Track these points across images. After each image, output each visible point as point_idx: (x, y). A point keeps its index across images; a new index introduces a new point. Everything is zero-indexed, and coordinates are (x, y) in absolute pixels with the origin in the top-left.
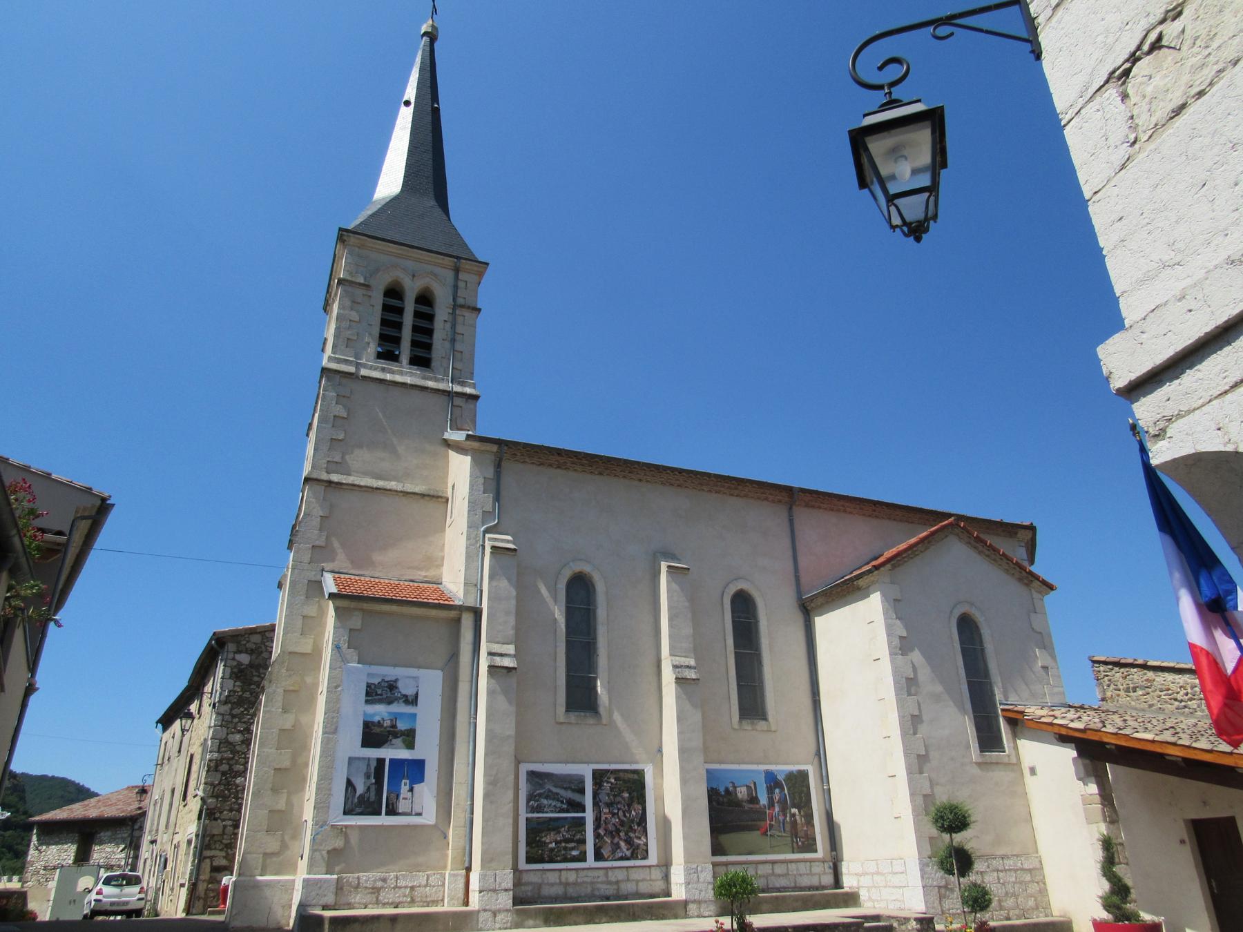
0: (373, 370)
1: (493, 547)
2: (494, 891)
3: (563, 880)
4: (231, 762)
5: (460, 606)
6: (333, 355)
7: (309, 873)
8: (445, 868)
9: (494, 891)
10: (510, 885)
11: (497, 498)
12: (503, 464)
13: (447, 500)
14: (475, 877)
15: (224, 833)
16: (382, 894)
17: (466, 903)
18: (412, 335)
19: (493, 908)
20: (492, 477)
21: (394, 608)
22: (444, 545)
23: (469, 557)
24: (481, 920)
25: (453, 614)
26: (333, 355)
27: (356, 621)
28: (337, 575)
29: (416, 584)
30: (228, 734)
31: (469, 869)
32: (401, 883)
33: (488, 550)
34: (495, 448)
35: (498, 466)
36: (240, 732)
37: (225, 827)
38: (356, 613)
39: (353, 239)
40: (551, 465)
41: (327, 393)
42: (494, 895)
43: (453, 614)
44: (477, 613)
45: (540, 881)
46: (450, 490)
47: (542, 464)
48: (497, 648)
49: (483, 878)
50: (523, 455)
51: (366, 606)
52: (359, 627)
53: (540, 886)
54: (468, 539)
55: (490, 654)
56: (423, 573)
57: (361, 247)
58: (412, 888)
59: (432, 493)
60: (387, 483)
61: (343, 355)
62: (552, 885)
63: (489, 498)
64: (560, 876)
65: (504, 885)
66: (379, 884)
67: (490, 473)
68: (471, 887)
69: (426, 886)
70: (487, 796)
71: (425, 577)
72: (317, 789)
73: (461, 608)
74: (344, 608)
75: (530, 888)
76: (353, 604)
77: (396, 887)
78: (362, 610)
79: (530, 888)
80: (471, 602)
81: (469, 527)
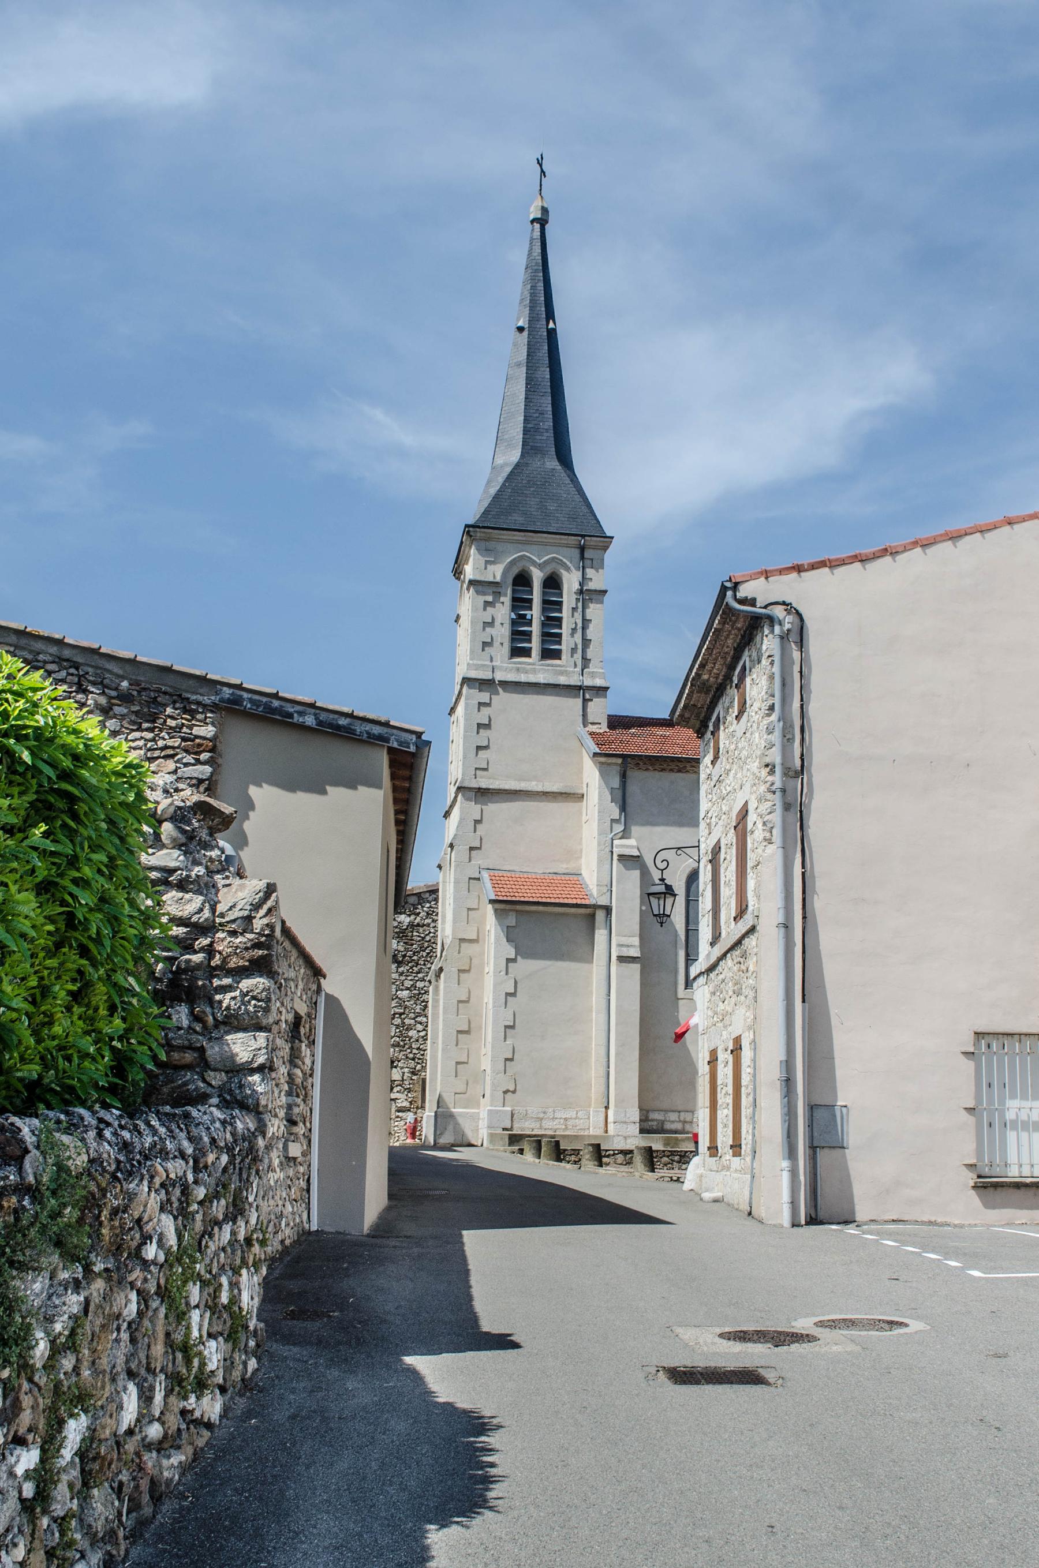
0: (507, 670)
1: (619, 856)
2: (625, 1122)
3: (682, 1119)
4: (403, 1016)
5: (594, 905)
6: (471, 662)
7: (491, 1106)
8: (590, 1106)
9: (625, 1122)
10: (637, 1119)
11: (623, 808)
12: (629, 773)
13: (583, 795)
14: (611, 1112)
15: (403, 1080)
16: (544, 1122)
17: (606, 1132)
18: (543, 592)
19: (624, 1134)
20: (618, 787)
21: (541, 908)
22: (581, 838)
23: (600, 861)
24: (615, 1142)
25: (588, 911)
26: (471, 662)
27: (511, 920)
28: (492, 873)
29: (559, 877)
30: (397, 991)
31: (607, 1108)
32: (558, 1115)
33: (615, 857)
34: (620, 761)
35: (624, 776)
36: (407, 989)
37: (404, 1073)
38: (511, 913)
39: (479, 533)
40: (671, 770)
41: (469, 701)
42: (625, 1126)
43: (588, 911)
44: (608, 910)
45: (663, 1118)
46: (585, 786)
47: (663, 770)
48: (624, 940)
49: (616, 1113)
50: (645, 764)
51: (519, 907)
52: (514, 924)
53: (663, 1122)
54: (599, 844)
55: (620, 945)
56: (565, 866)
57: (488, 539)
58: (566, 1119)
59: (568, 791)
60: (528, 783)
61: (480, 660)
62: (673, 1122)
63: (615, 812)
64: (679, 1116)
65: (632, 1119)
66: (541, 1115)
67: (616, 782)
68: (609, 1120)
69: (576, 1119)
70: (617, 1054)
71: (567, 868)
72: (493, 1047)
73: (596, 907)
74: (501, 910)
75: (655, 1123)
76: (508, 907)
77: (553, 1118)
78: (517, 911)
79: (655, 1123)
80: (603, 901)
81: (599, 834)
